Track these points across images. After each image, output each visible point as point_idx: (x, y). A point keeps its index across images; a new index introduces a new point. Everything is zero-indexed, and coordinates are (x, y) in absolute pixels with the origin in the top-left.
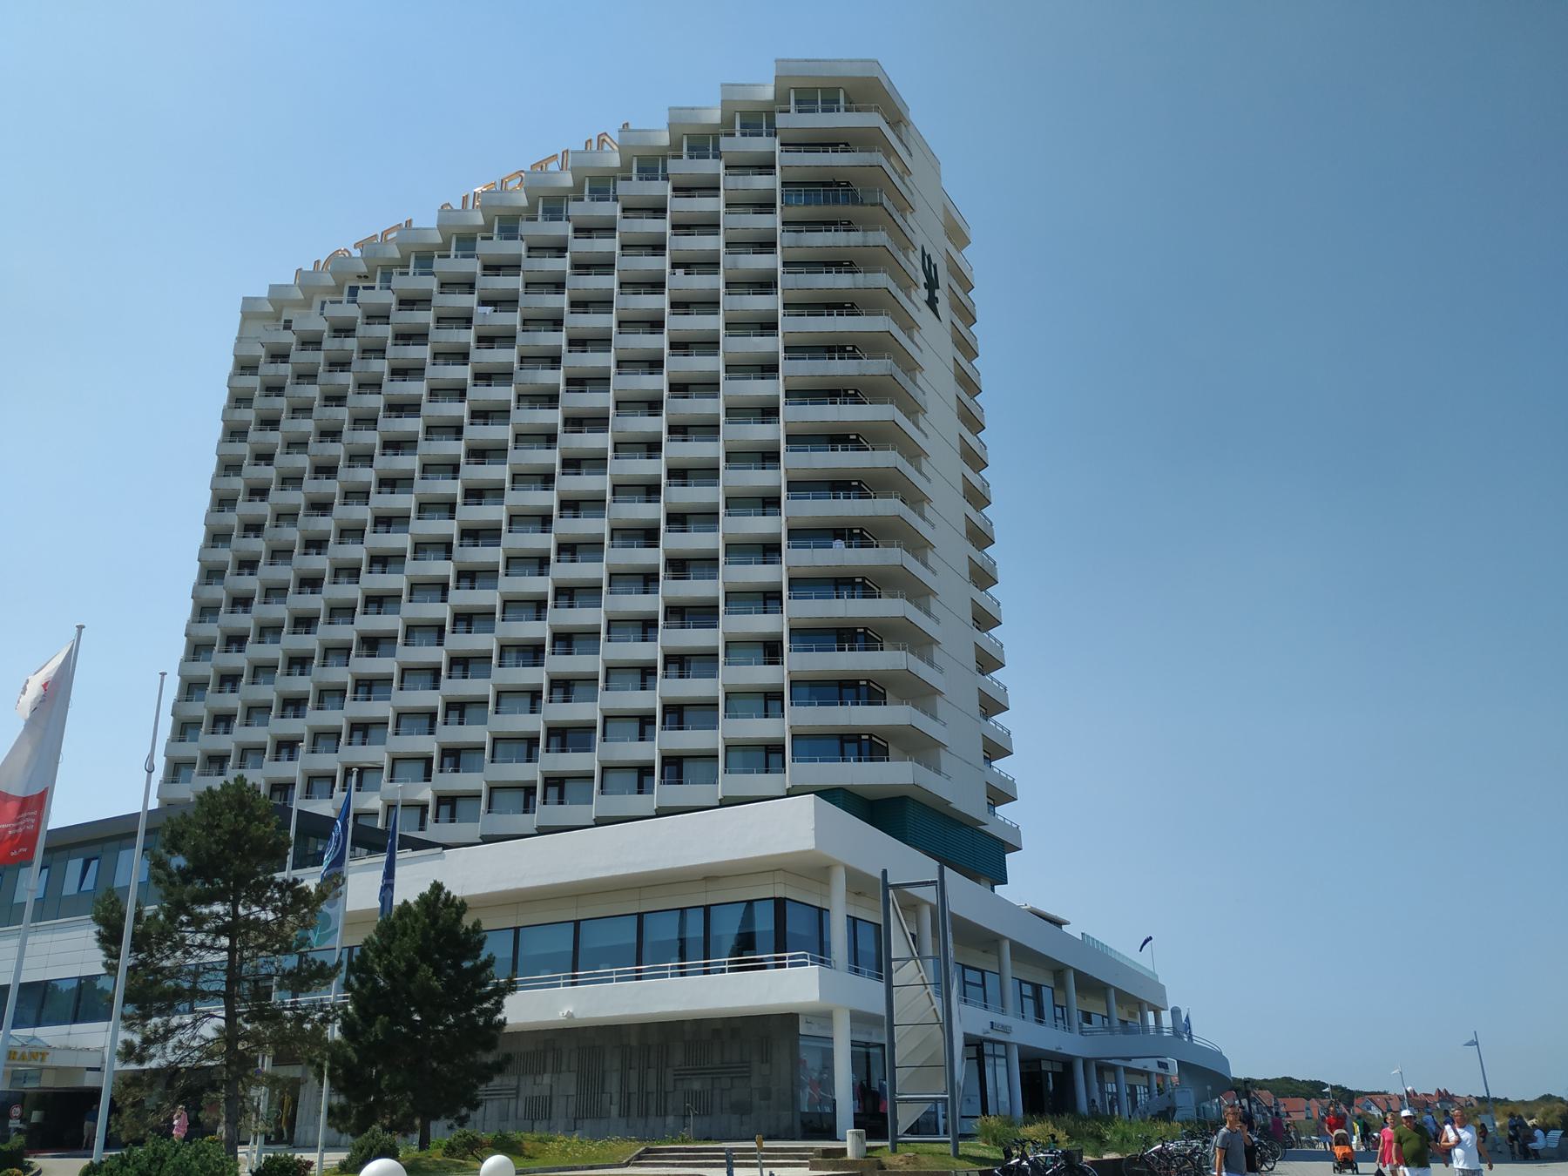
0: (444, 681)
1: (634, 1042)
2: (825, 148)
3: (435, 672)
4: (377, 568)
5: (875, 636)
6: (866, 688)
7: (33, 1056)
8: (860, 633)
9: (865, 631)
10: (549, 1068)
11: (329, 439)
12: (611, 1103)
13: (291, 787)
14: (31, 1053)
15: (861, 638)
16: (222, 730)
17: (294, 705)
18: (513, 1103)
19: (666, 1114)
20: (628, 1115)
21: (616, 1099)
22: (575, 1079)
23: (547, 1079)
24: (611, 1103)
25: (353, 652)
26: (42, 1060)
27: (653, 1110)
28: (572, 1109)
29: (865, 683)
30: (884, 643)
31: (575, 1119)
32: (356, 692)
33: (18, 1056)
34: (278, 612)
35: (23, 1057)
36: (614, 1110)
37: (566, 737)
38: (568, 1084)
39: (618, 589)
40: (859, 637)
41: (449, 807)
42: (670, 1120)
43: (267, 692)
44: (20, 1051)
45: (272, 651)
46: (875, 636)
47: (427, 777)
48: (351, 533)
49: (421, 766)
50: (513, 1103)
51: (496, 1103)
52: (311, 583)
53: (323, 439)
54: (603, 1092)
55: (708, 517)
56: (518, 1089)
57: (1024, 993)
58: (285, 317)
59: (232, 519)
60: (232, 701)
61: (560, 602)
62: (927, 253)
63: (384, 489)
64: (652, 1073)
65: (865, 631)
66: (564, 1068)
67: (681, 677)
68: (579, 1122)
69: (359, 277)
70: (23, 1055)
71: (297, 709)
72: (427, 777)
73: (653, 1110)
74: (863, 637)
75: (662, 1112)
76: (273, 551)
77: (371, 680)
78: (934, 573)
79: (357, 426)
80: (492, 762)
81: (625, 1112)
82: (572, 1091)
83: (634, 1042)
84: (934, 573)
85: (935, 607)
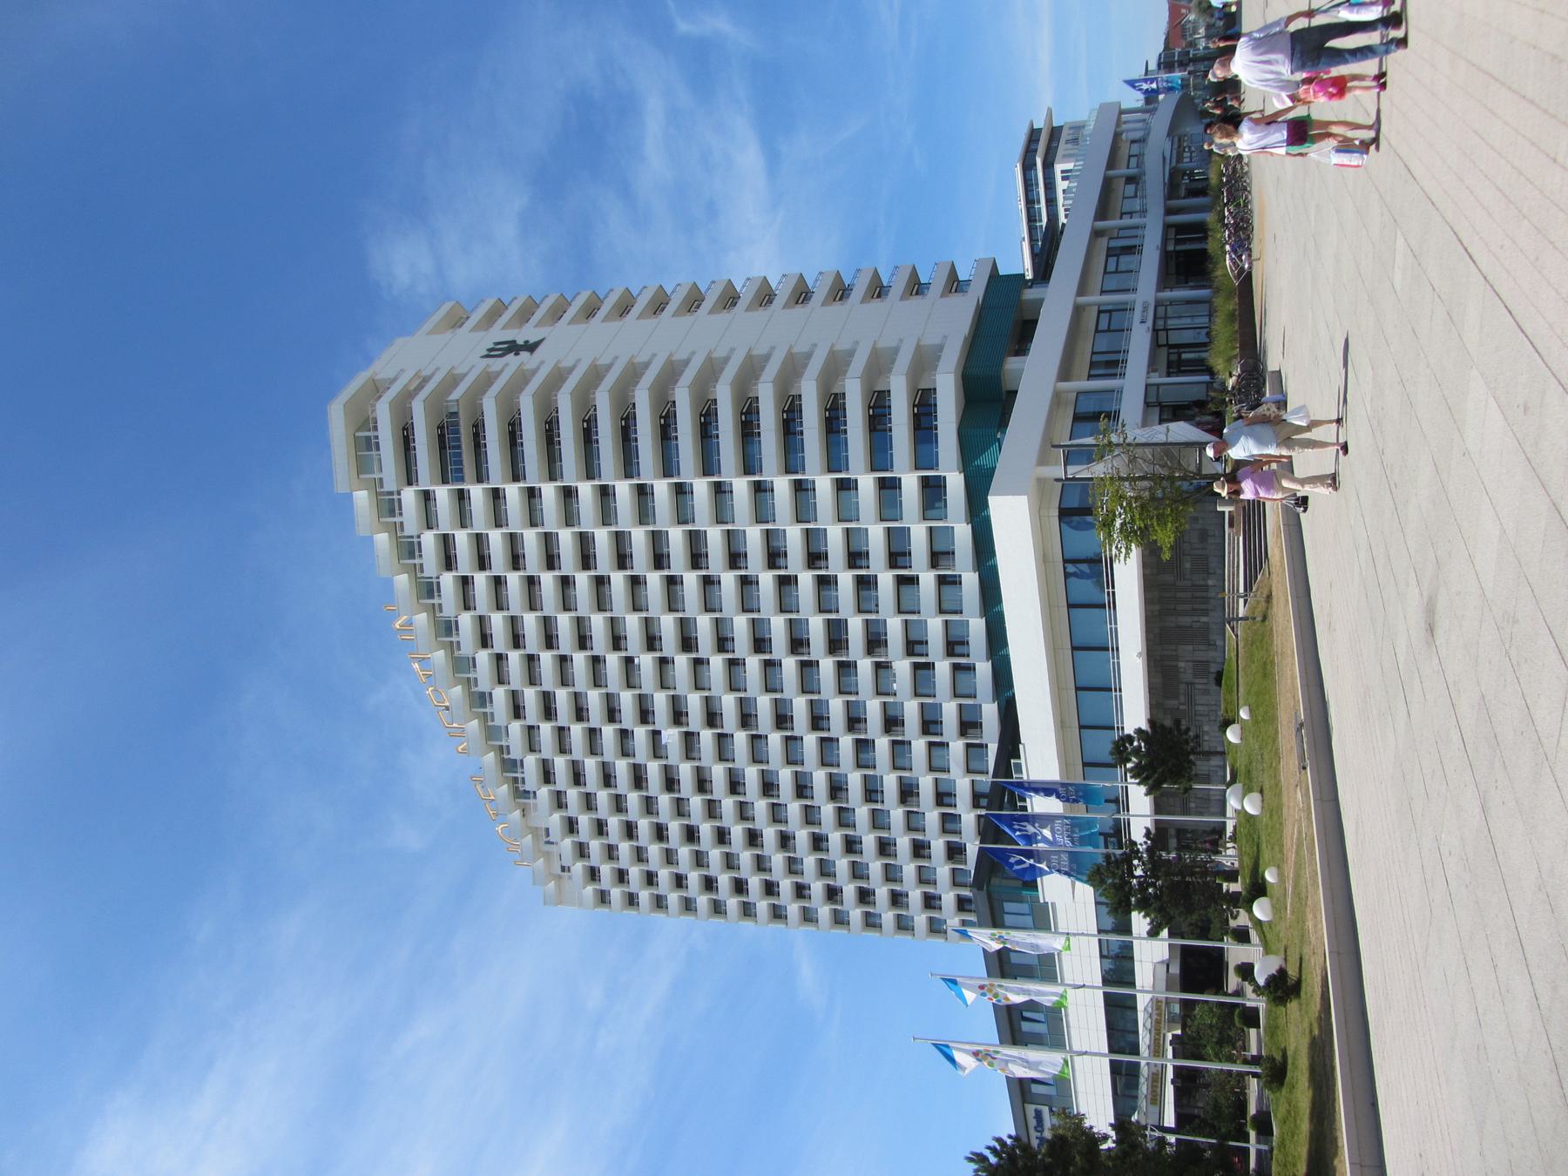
0: (796, 733)
1: (1157, 607)
2: (411, 441)
3: (755, 738)
4: (741, 789)
5: (919, 396)
6: (789, 414)
7: (1158, 1008)
8: (873, 412)
9: (663, 417)
10: (1174, 663)
11: (575, 826)
12: (1199, 621)
13: (848, 838)
14: (1157, 1009)
15: (708, 418)
16: (938, 902)
17: (753, 838)
18: (1198, 686)
19: (1207, 586)
20: (1207, 610)
21: (1196, 619)
22: (1183, 646)
23: (1182, 665)
24: (1199, 621)
25: (844, 805)
26: (1161, 1002)
27: (1204, 594)
28: (1201, 647)
29: (785, 415)
30: (751, 395)
31: (1209, 645)
32: (877, 802)
33: (1159, 1018)
34: (715, 855)
35: (1160, 1015)
36: (1204, 619)
37: (836, 640)
38: (1185, 650)
39: (644, 604)
40: (748, 419)
41: (930, 726)
42: (1210, 582)
43: (746, 857)
44: (1155, 1017)
45: (715, 855)
46: (919, 396)
47: (944, 745)
48: (619, 804)
49: (898, 747)
50: (1198, 686)
51: (1197, 697)
52: (630, 830)
53: (575, 830)
54: (1191, 627)
55: (657, 539)
56: (1187, 683)
57: (1106, 328)
58: (559, 871)
59: (673, 898)
60: (817, 888)
61: (730, 648)
62: (486, 353)
63: (613, 783)
64: (1179, 595)
65: (663, 417)
66: (1174, 653)
67: (786, 555)
68: (1211, 643)
69: (524, 815)
70: (1158, 1015)
71: (855, 842)
72: (944, 745)
73: (1204, 594)
74: (748, 416)
75: (1206, 588)
76: (639, 861)
77: (866, 790)
78: (616, 358)
79: (594, 807)
80: (935, 696)
81: (1206, 612)
82: (1190, 648)
83: (1157, 607)
84: (616, 358)
85: (567, 363)
